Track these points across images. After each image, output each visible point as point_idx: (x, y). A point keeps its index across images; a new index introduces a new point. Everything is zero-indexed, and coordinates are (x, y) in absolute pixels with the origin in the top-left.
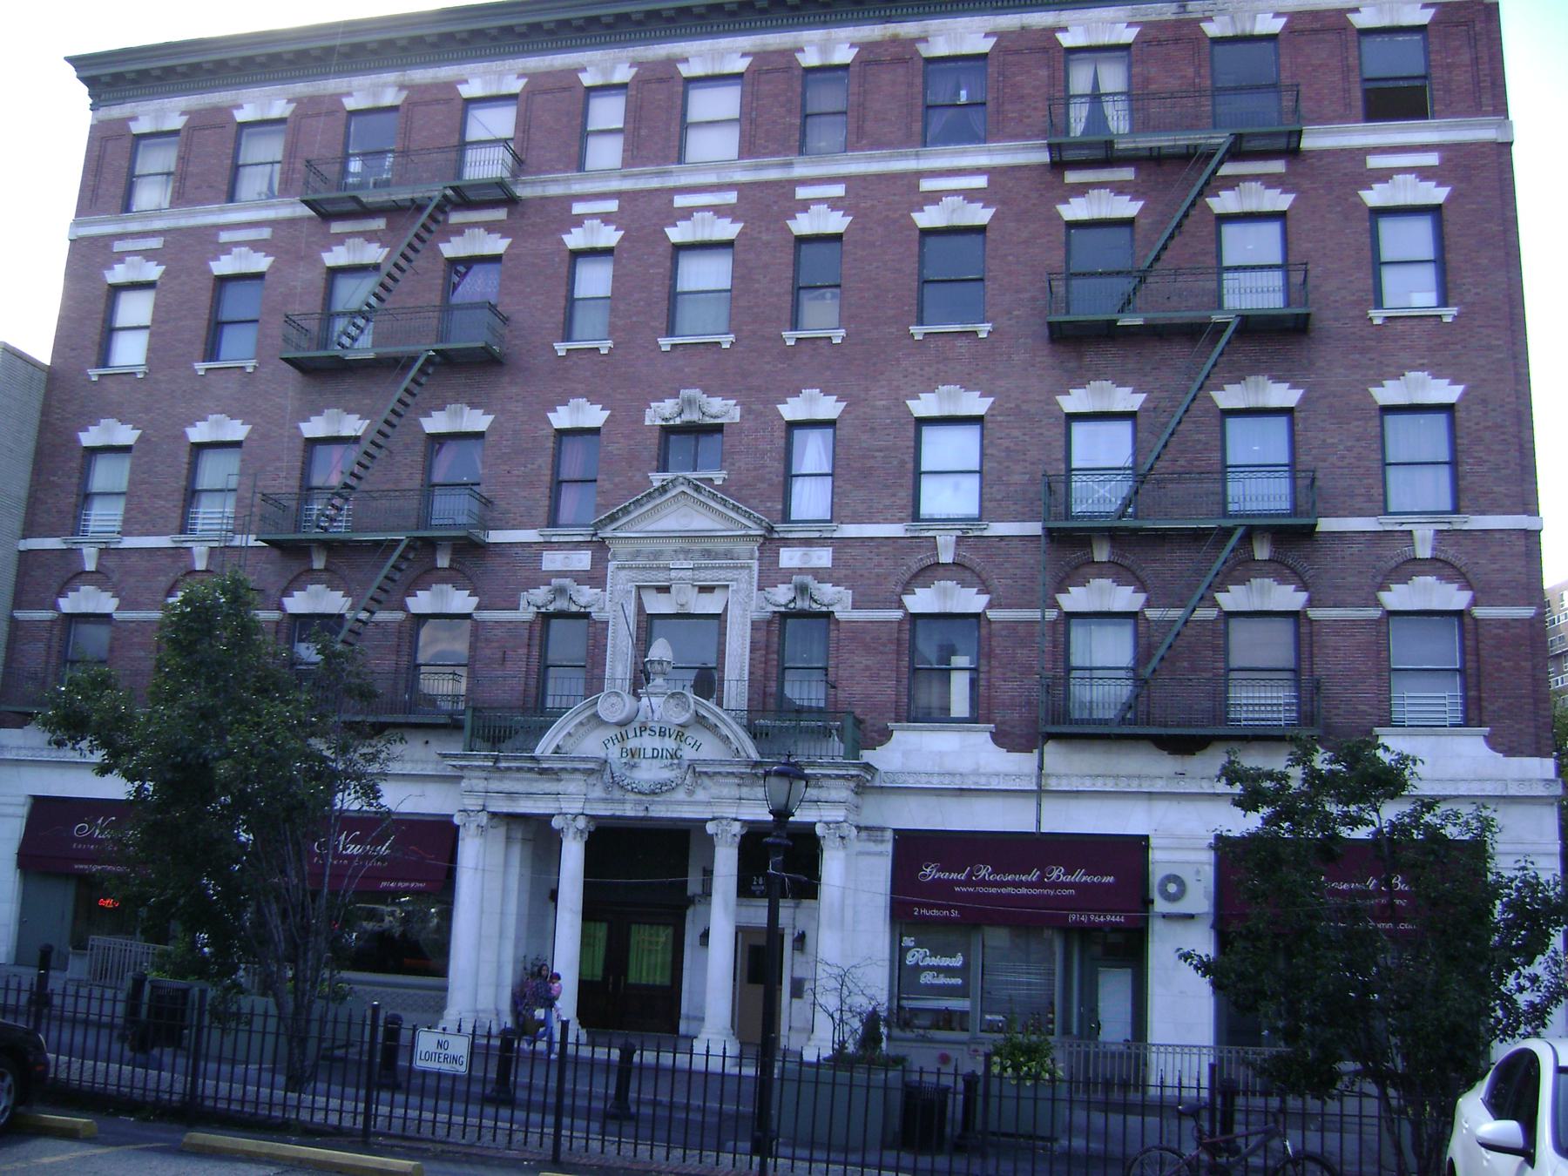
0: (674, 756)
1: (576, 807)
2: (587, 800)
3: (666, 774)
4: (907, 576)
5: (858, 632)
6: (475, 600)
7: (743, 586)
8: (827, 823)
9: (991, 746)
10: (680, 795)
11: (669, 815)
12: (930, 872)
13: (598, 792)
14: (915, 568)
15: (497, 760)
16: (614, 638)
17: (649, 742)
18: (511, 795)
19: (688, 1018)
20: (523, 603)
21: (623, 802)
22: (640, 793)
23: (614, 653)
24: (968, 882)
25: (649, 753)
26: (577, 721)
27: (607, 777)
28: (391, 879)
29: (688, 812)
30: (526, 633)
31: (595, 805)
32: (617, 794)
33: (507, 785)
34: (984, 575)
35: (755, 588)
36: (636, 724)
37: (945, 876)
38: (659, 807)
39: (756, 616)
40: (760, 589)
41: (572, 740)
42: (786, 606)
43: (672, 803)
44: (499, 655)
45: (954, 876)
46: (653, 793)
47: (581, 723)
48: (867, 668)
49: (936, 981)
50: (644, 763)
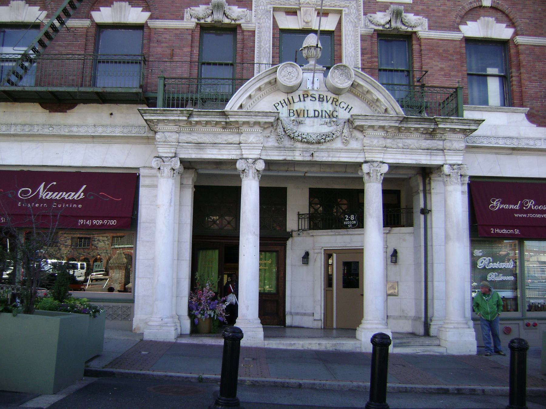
0: (331, 116)
1: (254, 154)
2: (264, 148)
3: (326, 129)
4: (463, 13)
5: (434, 44)
6: (148, 14)
7: (353, 11)
8: (451, 165)
9: (526, 122)
10: (338, 144)
11: (330, 159)
12: (496, 204)
13: (272, 142)
14: (467, 7)
15: (190, 115)
16: (260, 42)
17: (310, 106)
18: (199, 145)
19: (291, 313)
20: (187, 16)
21: (293, 149)
22: (308, 143)
23: (259, 52)
24: (521, 211)
25: (311, 114)
26: (257, 86)
27: (280, 130)
28: (86, 218)
29: (344, 158)
30: (189, 37)
31: (270, 152)
32: (287, 143)
33: (195, 137)
34: (511, 16)
35: (362, 13)
36: (300, 92)
37: (506, 207)
38: (322, 154)
39: (364, 31)
40: (365, 14)
41: (251, 101)
42: (383, 26)
43: (332, 150)
44: (169, 52)
45: (512, 207)
46: (319, 143)
47: (260, 89)
48: (442, 69)
49: (498, 279)
50: (308, 121)
